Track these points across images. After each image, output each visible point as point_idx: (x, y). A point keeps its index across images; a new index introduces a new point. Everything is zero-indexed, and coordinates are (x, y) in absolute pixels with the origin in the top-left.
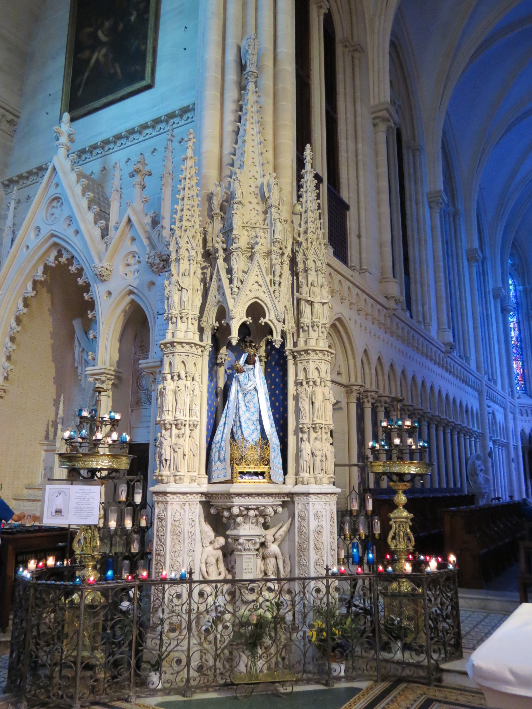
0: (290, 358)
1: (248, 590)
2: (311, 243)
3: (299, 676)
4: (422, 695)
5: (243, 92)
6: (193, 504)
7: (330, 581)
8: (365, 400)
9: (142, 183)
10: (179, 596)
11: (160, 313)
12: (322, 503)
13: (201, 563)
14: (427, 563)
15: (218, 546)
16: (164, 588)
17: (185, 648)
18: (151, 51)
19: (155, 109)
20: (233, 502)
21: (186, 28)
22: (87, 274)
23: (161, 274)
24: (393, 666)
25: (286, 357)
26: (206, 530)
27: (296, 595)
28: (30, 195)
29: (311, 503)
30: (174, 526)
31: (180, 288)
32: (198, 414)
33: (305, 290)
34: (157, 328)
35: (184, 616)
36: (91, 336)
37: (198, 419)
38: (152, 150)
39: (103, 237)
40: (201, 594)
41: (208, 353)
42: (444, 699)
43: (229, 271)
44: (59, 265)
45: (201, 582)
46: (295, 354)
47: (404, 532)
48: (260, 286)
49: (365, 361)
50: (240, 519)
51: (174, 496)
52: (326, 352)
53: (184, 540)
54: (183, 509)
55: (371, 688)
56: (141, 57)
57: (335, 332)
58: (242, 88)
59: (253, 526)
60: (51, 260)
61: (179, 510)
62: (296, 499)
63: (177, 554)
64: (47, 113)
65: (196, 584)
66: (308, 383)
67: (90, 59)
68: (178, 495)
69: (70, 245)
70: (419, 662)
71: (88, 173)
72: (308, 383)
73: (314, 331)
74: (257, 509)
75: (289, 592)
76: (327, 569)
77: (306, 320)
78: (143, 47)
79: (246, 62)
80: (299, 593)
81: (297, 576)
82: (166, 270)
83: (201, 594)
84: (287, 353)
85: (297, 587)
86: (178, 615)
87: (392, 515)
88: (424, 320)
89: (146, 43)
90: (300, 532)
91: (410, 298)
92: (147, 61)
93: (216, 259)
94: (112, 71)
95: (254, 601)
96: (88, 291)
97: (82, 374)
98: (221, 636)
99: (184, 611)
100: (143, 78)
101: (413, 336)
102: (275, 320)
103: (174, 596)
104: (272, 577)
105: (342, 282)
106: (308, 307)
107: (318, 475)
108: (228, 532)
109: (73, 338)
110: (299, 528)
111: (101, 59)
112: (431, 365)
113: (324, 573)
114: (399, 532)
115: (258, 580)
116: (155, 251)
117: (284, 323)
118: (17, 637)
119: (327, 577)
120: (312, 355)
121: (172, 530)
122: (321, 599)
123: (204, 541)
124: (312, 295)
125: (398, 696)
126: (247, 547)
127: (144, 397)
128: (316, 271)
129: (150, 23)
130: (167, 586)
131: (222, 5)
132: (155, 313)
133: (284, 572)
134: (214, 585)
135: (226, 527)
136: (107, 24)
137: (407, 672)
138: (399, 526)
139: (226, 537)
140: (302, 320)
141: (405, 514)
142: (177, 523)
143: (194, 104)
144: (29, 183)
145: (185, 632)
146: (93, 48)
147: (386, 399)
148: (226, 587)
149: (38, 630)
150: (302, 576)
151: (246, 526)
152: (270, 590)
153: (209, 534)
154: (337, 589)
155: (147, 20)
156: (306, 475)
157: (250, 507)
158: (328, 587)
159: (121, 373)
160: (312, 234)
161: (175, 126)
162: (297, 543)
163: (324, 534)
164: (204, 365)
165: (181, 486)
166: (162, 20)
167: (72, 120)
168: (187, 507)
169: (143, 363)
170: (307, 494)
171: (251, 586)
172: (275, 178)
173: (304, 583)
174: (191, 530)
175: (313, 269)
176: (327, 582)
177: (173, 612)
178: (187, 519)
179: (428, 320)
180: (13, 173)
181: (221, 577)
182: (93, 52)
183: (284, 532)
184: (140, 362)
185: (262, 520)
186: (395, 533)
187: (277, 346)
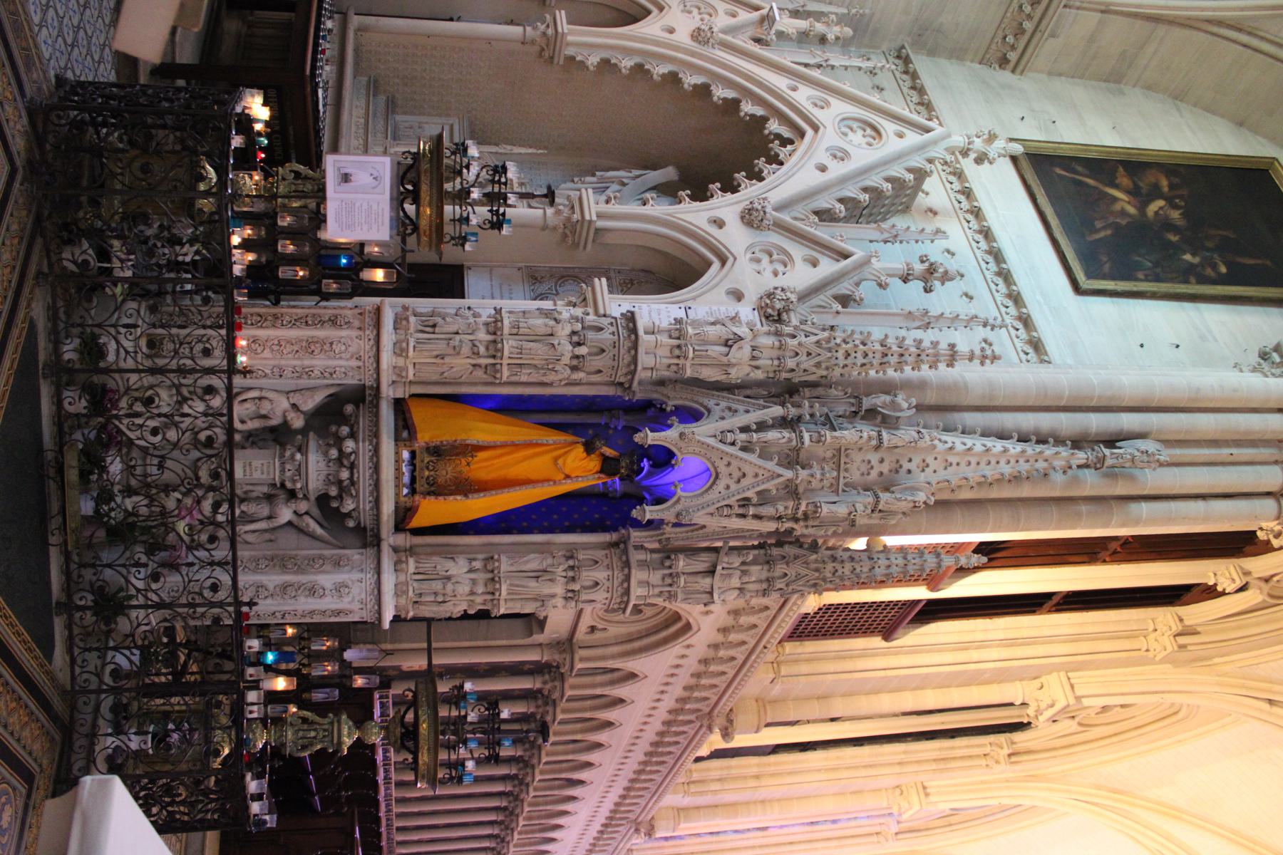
0: (614, 537)
1: (217, 468)
2: (817, 570)
3: (76, 558)
4: (40, 766)
5: (1069, 443)
6: (360, 374)
7: (231, 609)
8: (547, 677)
9: (910, 278)
10: (207, 353)
11: (689, 311)
12: (363, 596)
13: (261, 389)
14: (258, 776)
15: (289, 418)
16: (221, 327)
17: (122, 365)
18: (1135, 289)
19: (1039, 297)
20: (364, 441)
21: (1178, 346)
22: (753, 188)
23: (756, 312)
24: (89, 718)
25: (616, 530)
26: (316, 397)
27: (208, 550)
28: (884, 92)
29: (362, 575)
30: (323, 342)
31: (730, 343)
32: (514, 379)
33: (736, 561)
34: (663, 306)
35: (175, 361)
36: (648, 195)
37: (504, 379)
38: (970, 294)
39: (816, 213)
40: (210, 390)
41: (619, 394)
42: (32, 803)
43: (762, 426)
44: (767, 140)
45: (229, 388)
46: (622, 546)
47: (315, 738)
48: (739, 481)
49: (616, 675)
50: (334, 453)
51: (372, 342)
52: (625, 599)
53: (299, 359)
54: (352, 357)
55: (53, 679)
56: (1125, 273)
57: (666, 620)
58: (1078, 443)
59: (322, 477)
60: (774, 126)
61: (350, 349)
62: (371, 552)
63: (276, 348)
64: (1023, 118)
65: (226, 381)
66: (572, 568)
67: (1116, 187)
68: (374, 349)
69: (802, 158)
70: (94, 762)
71: (926, 186)
72: (572, 568)
73: (663, 579)
74: (353, 483)
75: (213, 539)
76: (251, 604)
77: (681, 563)
78: (1140, 275)
79: (1120, 448)
80: (211, 556)
81: (239, 553)
82: (763, 319)
83: (210, 390)
84: (623, 531)
85: (221, 553)
86: (176, 352)
87: (344, 717)
88: (694, 782)
89: (1147, 280)
90: (313, 559)
91: (733, 756)
92: (1118, 283)
93: (783, 404)
94: (1098, 224)
95: (198, 478)
96: (724, 190)
97: (583, 183)
98: (141, 426)
99: (182, 362)
100: (1089, 276)
101: (663, 763)
102: (679, 507)
103: (207, 345)
104: (237, 512)
105: (754, 631)
106: (702, 566)
107: (411, 589)
108: (311, 434)
109: (646, 168)
110: (320, 557)
111: (1117, 207)
112: (613, 797)
113: (246, 599)
114: (315, 730)
115: (232, 487)
116: (794, 300)
117: (676, 525)
118: (145, 93)
119: (238, 603)
120: (619, 576)
121: (315, 340)
122: (201, 594)
123: (297, 394)
124: (724, 572)
125: (39, 724)
126: (288, 466)
127: (543, 288)
128: (768, 580)
129: (1183, 286)
130: (223, 332)
131: (1211, 405)
132: (689, 304)
133: (246, 532)
134: (225, 411)
135: (323, 432)
136: (1175, 214)
137: (80, 742)
138: (325, 730)
139: (304, 431)
140: (681, 556)
141: (347, 742)
142: (327, 347)
143: (1050, 363)
144: (905, 90)
145: (148, 363)
146: (1134, 192)
147: (551, 713)
148: (220, 435)
149: (154, 126)
150: (239, 563)
151: (322, 465)
152: (216, 506)
153: (310, 401)
154: (217, 620)
155: (1186, 282)
156: (412, 568)
157: (355, 471)
158: (221, 604)
159: (585, 248)
160: (833, 570)
161: (1013, 332)
162: (294, 552)
163: (310, 600)
164: (599, 387)
165: (390, 353)
166: (1187, 306)
167: (1014, 159)
168: (354, 363)
169: (601, 284)
170: (378, 571)
171: (223, 474)
172: (925, 503)
173: (227, 563)
174: (316, 372)
175: (770, 574)
176: (230, 604)
177: (181, 344)
178: (336, 363)
179: (693, 788)
180: (921, 64)
181: (237, 425)
182: (1128, 192)
183: (314, 531)
184: (604, 280)
185: (333, 492)
186: (313, 723)
187: (635, 513)
